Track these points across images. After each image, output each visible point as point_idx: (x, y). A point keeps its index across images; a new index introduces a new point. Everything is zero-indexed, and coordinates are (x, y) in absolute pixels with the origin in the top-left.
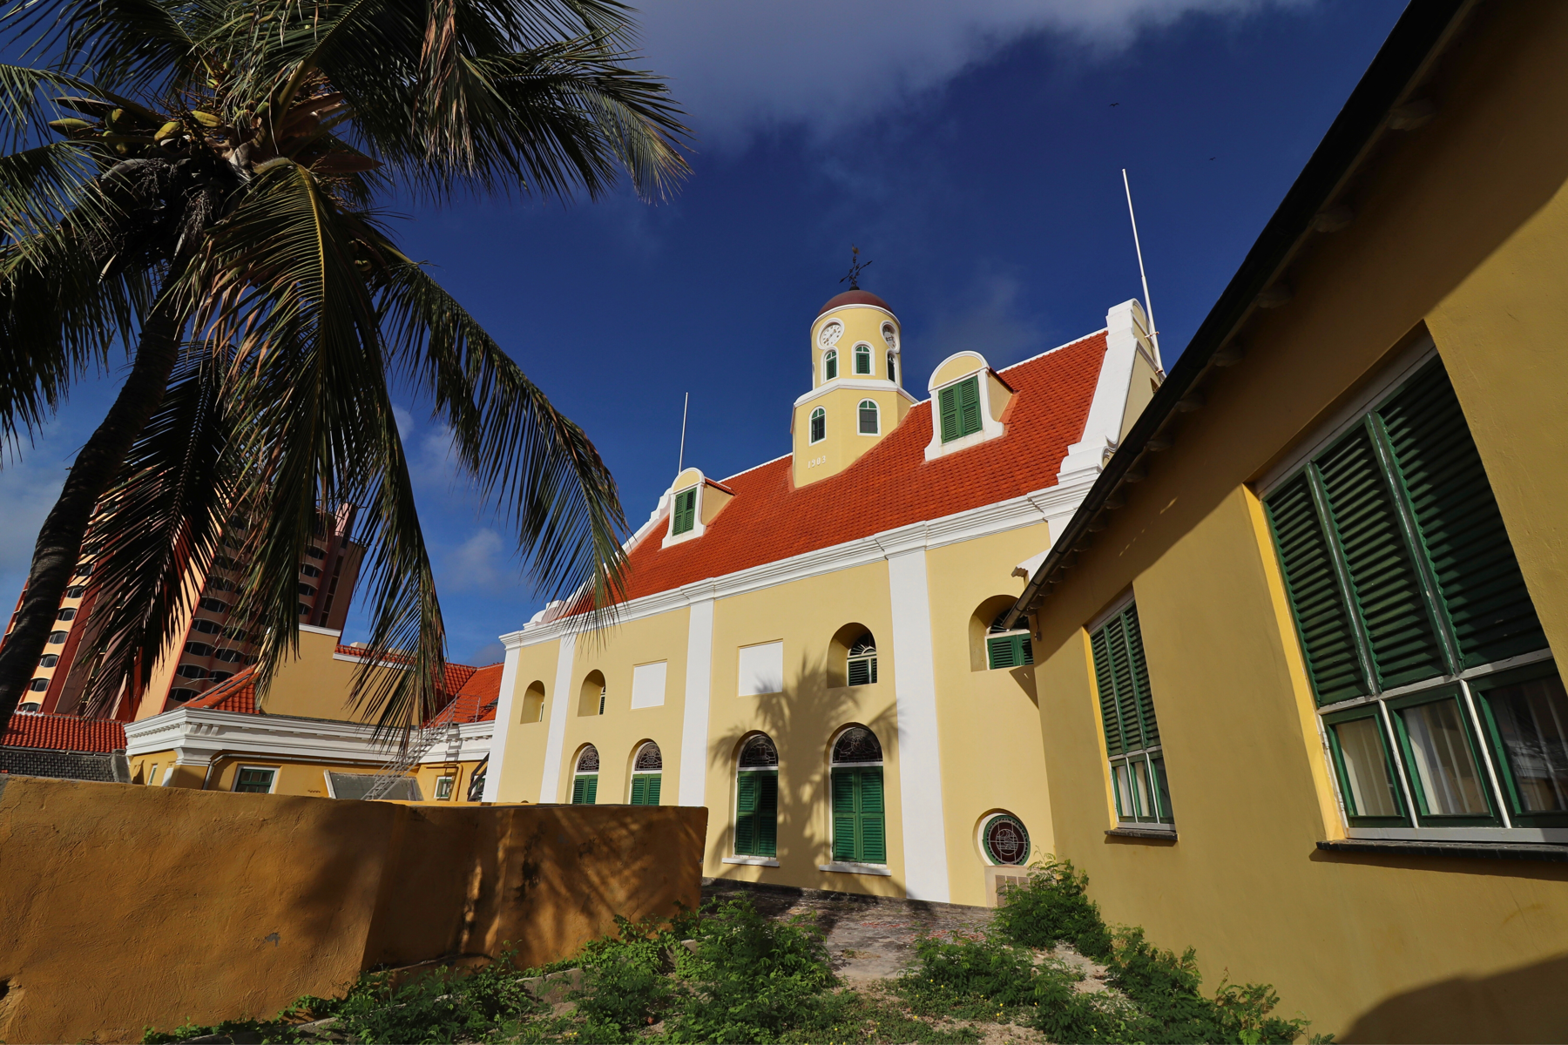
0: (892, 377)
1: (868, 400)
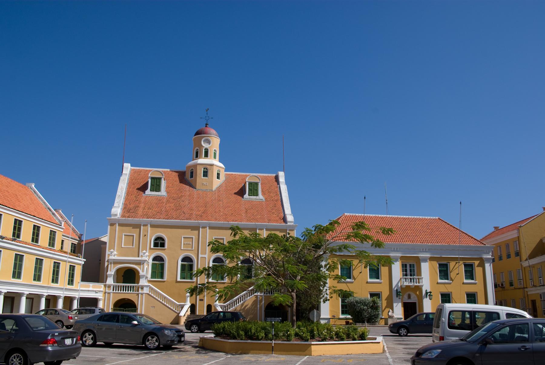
0: (215, 157)
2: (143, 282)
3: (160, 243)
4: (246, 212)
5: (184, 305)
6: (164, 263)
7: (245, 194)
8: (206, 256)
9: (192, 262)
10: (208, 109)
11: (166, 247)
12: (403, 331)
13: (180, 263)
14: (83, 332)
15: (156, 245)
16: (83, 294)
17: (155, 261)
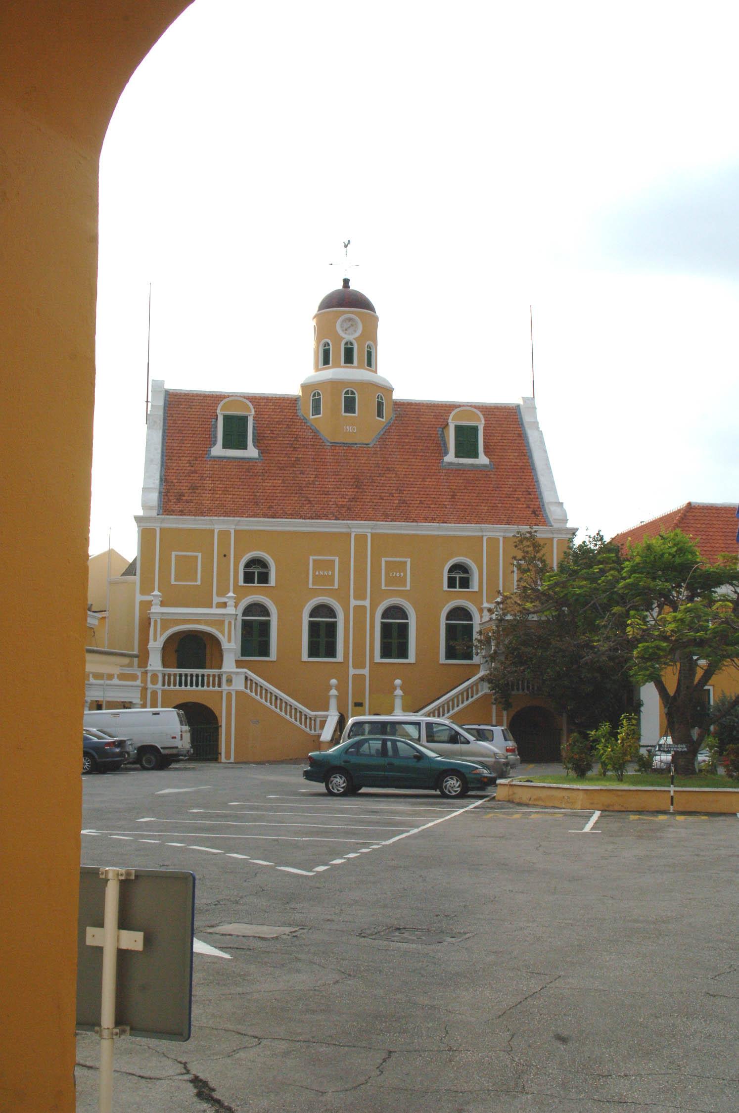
1: (350, 389)
2: (229, 665)
3: (460, 578)
4: (453, 496)
5: (327, 717)
6: (336, 622)
7: (446, 453)
8: (367, 603)
9: (335, 617)
10: (349, 242)
11: (475, 586)
12: (339, 782)
13: (306, 619)
14: (454, 769)
15: (248, 578)
16: (112, 694)
17: (385, 619)
